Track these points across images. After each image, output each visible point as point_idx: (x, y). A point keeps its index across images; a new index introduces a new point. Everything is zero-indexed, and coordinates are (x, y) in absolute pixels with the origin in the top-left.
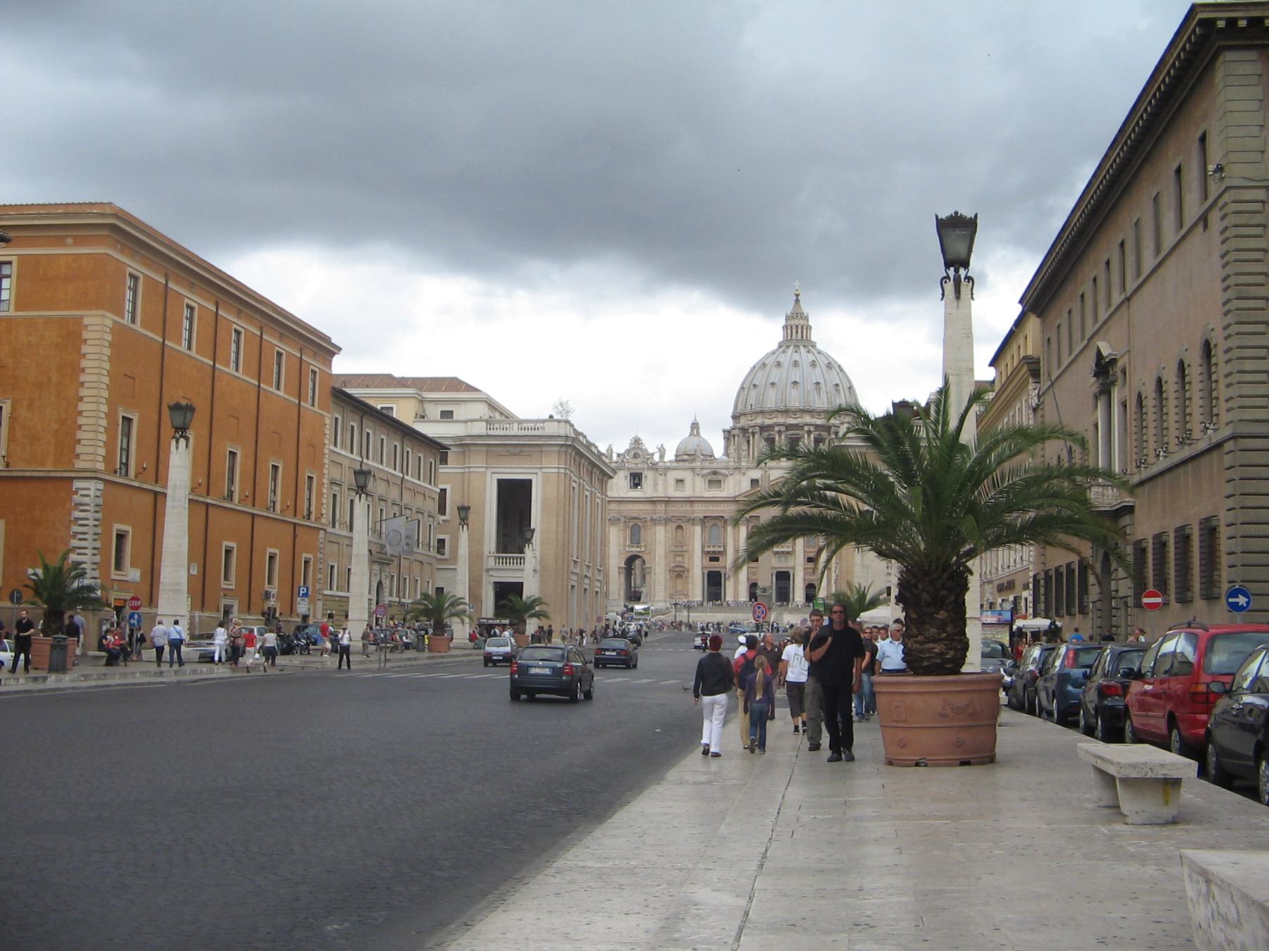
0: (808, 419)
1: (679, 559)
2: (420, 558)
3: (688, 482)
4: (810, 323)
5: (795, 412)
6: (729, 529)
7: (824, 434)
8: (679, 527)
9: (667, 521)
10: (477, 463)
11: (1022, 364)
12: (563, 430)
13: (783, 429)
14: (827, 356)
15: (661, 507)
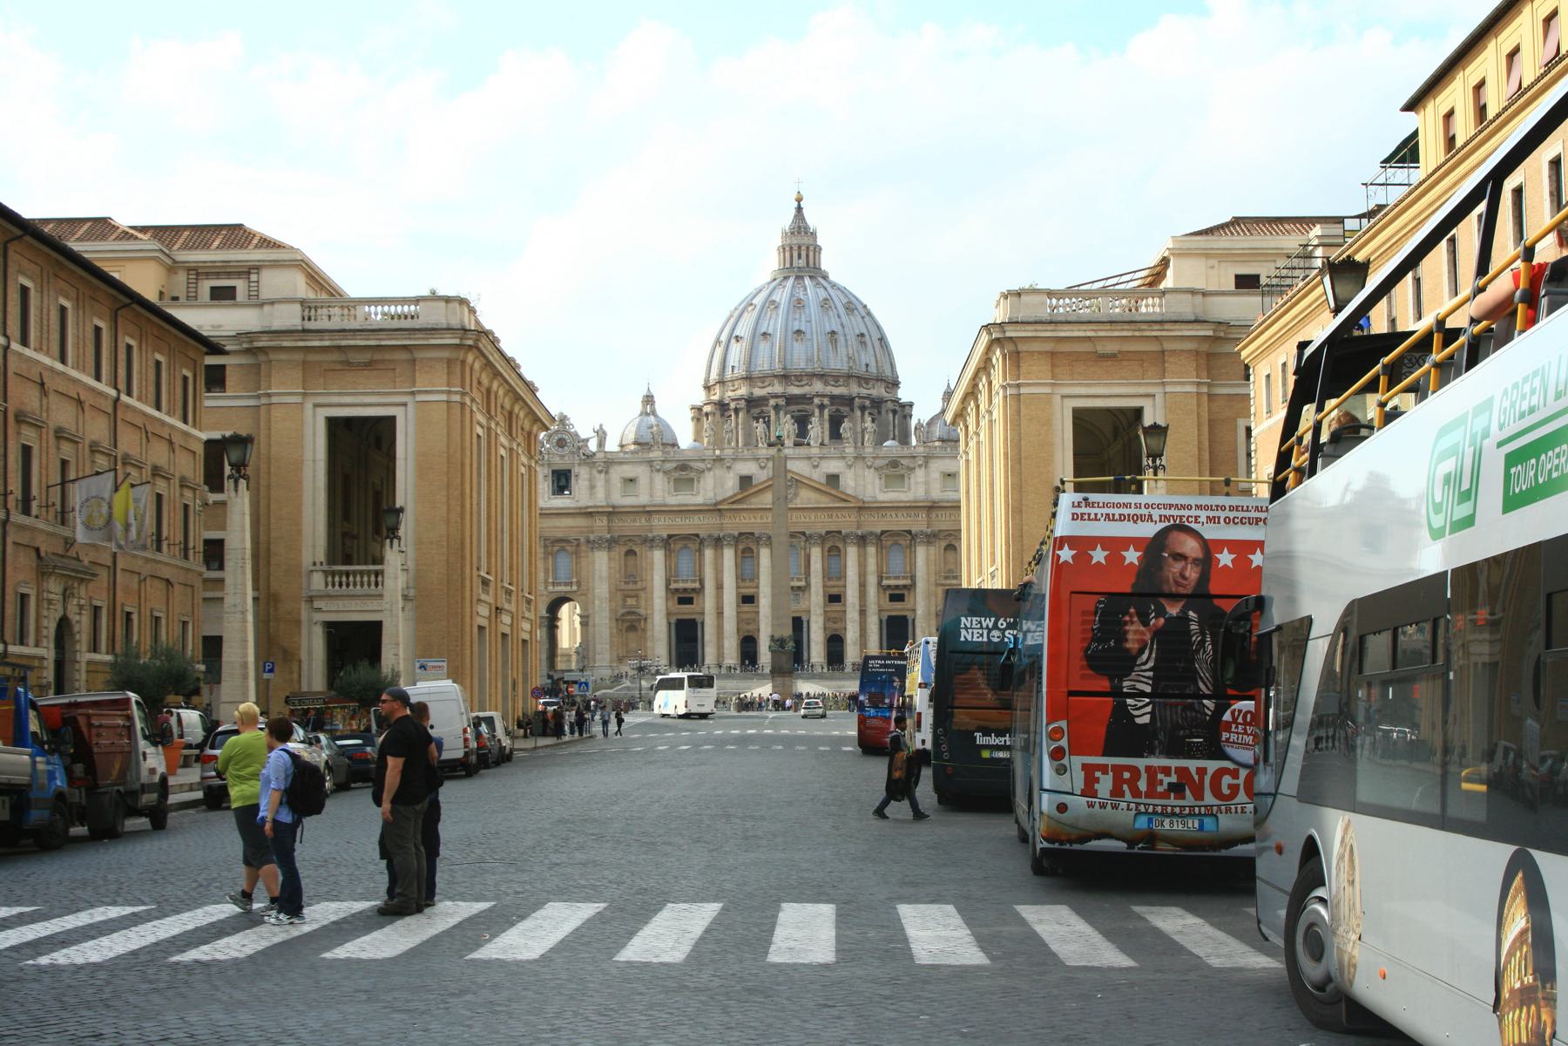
0: (818, 387)
1: (631, 601)
2: (166, 573)
3: (643, 482)
5: (799, 378)
6: (709, 553)
7: (844, 409)
8: (631, 553)
9: (611, 543)
10: (284, 388)
11: (334, 777)
12: (456, 318)
13: (782, 402)
14: (843, 290)
15: (601, 522)
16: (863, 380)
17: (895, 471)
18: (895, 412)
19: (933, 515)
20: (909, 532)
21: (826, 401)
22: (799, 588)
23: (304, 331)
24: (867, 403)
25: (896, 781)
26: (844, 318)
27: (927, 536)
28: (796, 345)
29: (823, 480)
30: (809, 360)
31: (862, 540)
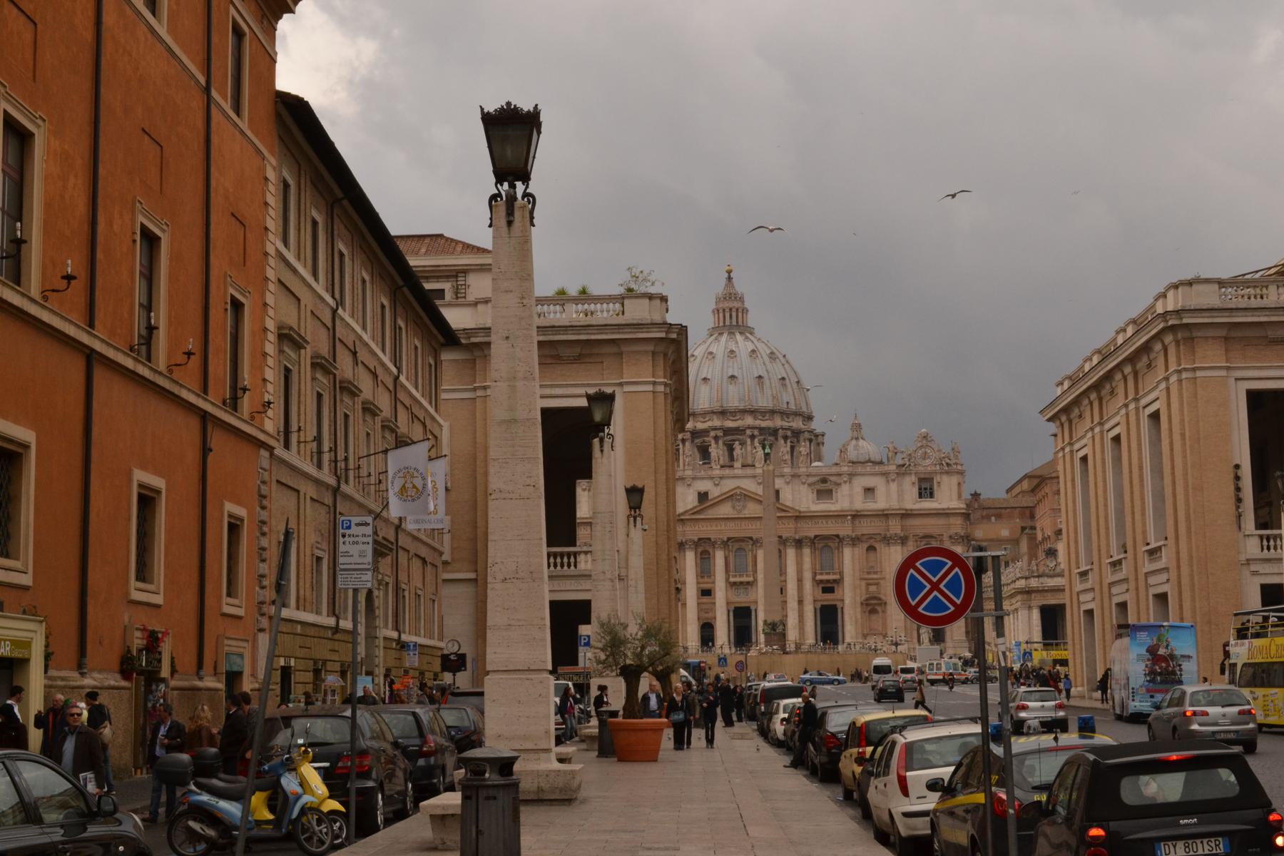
0: (749, 421)
1: (873, 588)
4: (747, 305)
8: (871, 548)
9: (855, 541)
13: (720, 433)
16: (784, 414)
17: (824, 488)
18: (811, 441)
19: (857, 522)
20: (837, 536)
21: (756, 432)
22: (748, 583)
24: (789, 433)
25: (922, 747)
26: (769, 366)
27: (853, 539)
28: (731, 387)
30: (740, 400)
31: (799, 543)
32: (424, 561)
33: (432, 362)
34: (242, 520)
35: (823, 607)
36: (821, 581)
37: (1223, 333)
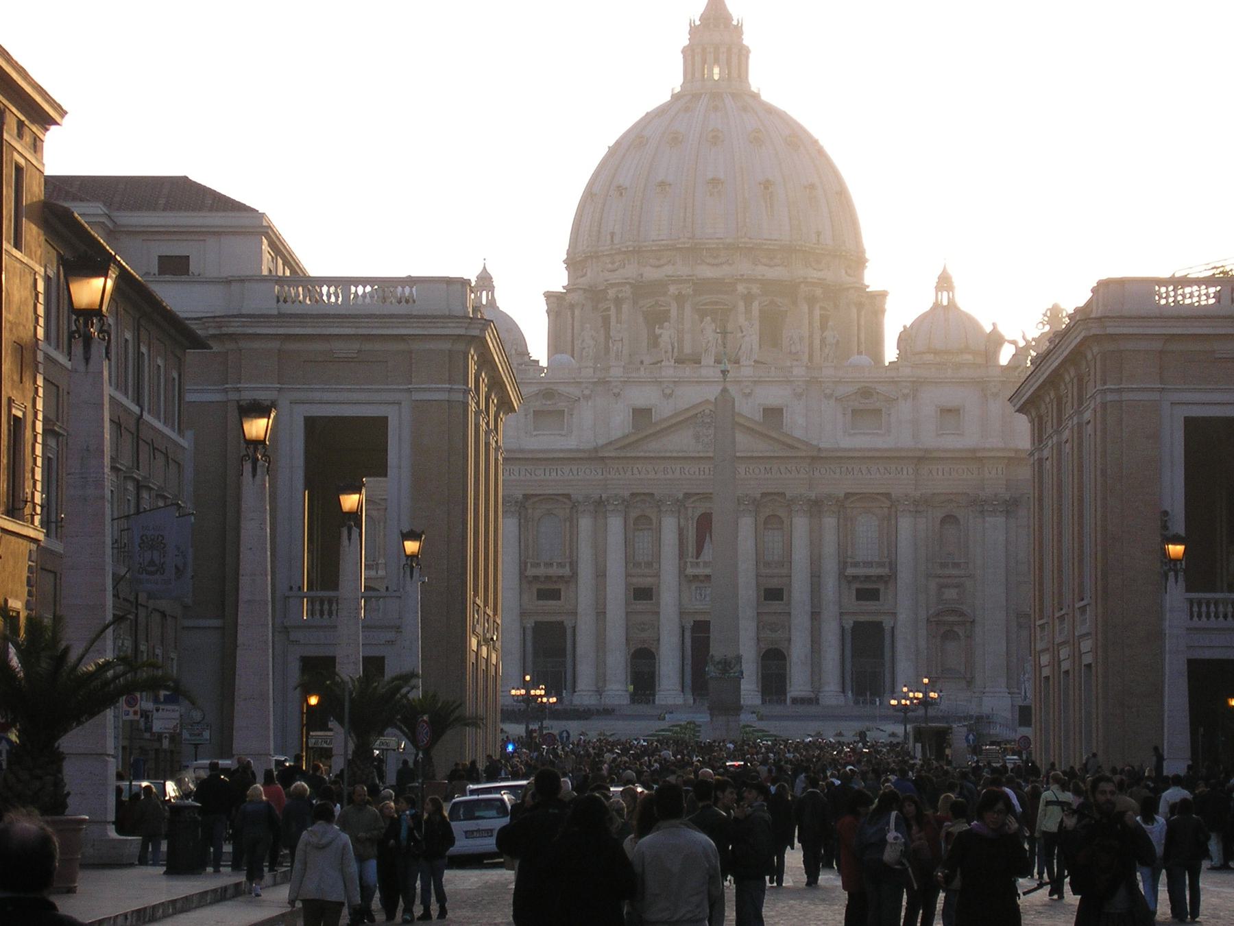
6: (585, 523)
13: (688, 290)
23: (281, 315)
29: (758, 417)
32: (164, 615)
33: (176, 375)
34: (18, 613)
35: (857, 626)
36: (855, 578)
37: (1157, 345)
